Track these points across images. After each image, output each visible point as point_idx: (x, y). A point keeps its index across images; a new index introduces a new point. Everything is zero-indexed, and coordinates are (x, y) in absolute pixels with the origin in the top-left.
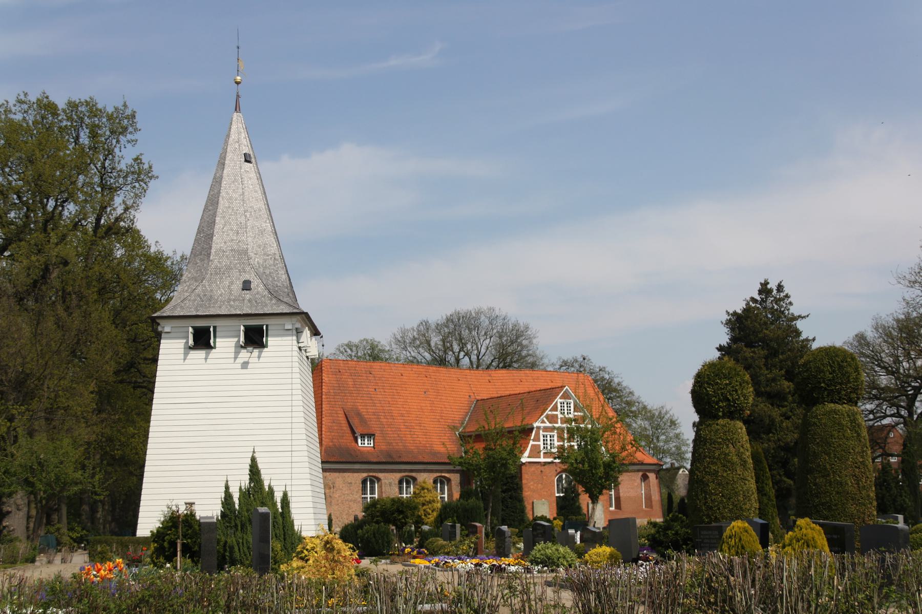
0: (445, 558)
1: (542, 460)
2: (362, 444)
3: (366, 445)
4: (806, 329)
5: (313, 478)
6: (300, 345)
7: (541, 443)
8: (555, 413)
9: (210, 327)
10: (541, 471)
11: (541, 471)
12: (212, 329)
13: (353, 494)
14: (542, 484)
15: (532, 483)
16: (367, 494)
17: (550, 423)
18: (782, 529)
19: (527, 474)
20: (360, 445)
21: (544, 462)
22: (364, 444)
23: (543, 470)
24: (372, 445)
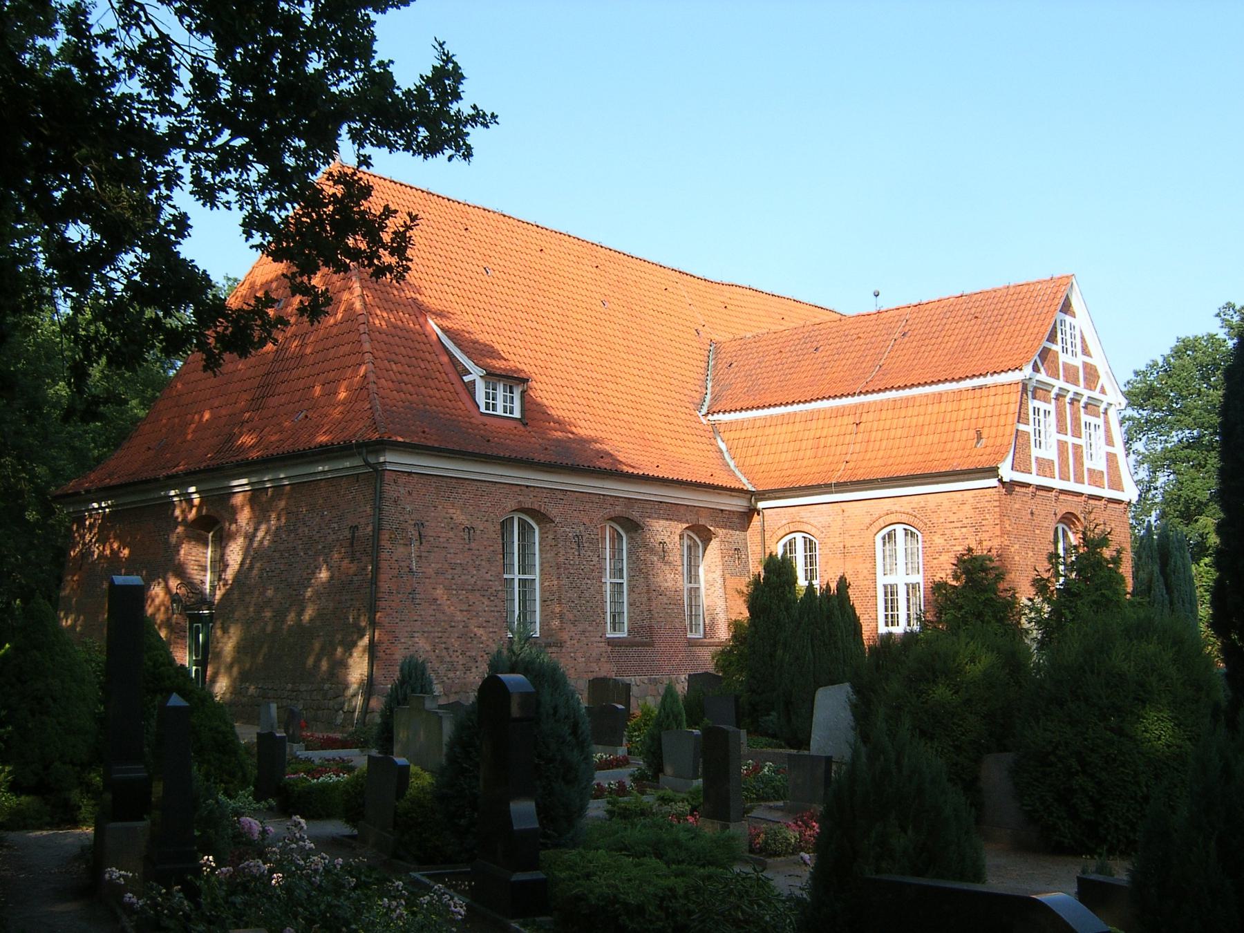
3: (500, 412)
13: (478, 568)
24: (517, 414)
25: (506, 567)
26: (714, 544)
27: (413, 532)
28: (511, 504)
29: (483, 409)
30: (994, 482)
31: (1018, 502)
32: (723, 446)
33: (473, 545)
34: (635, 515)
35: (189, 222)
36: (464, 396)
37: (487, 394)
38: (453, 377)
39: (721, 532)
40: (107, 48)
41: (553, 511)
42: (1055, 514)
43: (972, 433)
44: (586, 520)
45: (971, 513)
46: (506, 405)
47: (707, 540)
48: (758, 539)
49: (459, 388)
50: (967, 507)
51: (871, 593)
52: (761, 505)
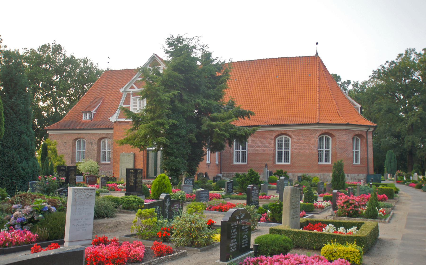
17: (138, 88)
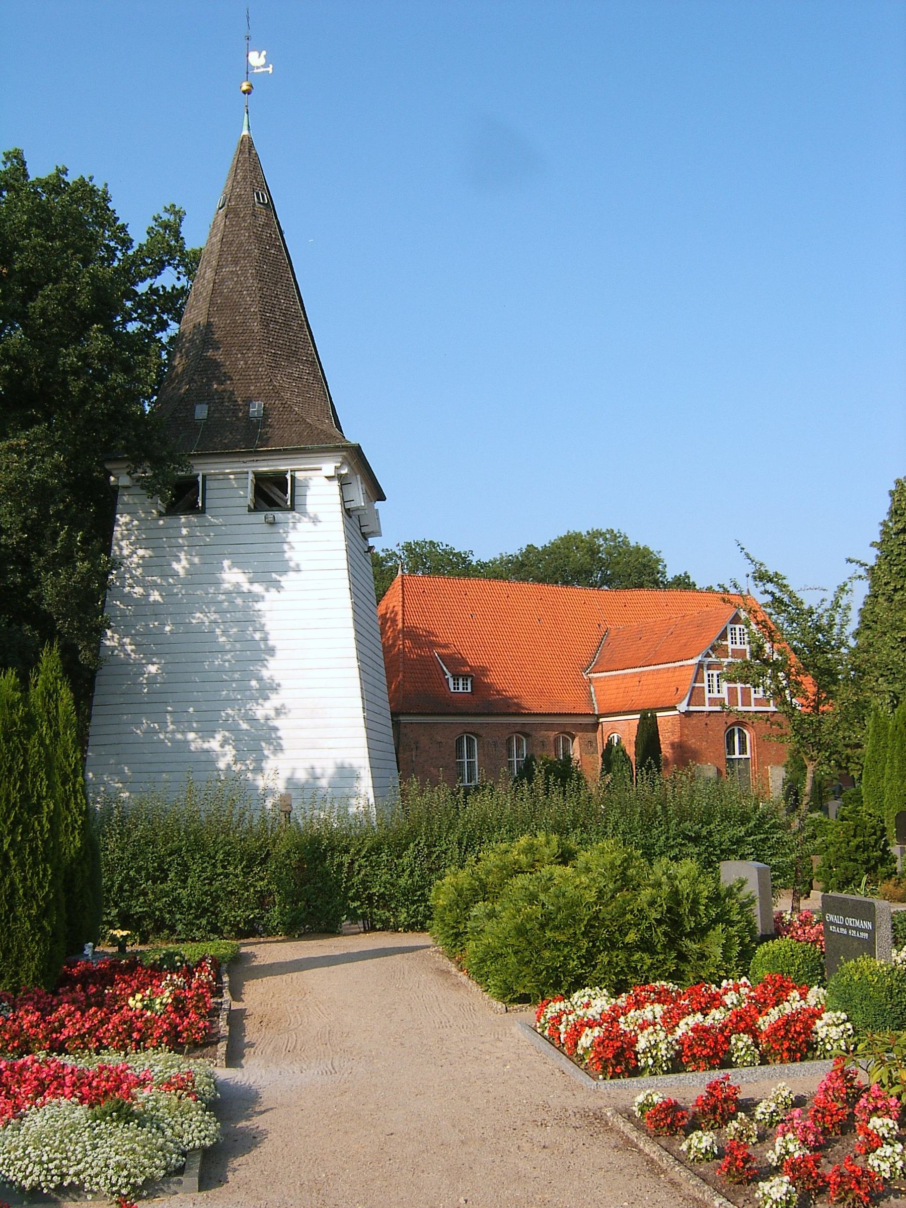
0: (338, 894)
1: (707, 708)
2: (455, 689)
3: (461, 690)
4: (251, 982)
5: (376, 709)
6: (348, 506)
7: (706, 685)
8: (724, 643)
9: (198, 475)
10: (706, 724)
11: (706, 724)
12: (200, 479)
14: (707, 741)
15: (693, 741)
16: (462, 757)
18: (565, 857)
19: (687, 728)
20: (452, 690)
21: (710, 712)
22: (458, 689)
23: (708, 722)
24: (469, 690)
25: (462, 757)
26: (577, 739)
27: (414, 746)
28: (460, 731)
29: (452, 690)
30: (677, 712)
31: (694, 720)
32: (592, 689)
33: (442, 749)
34: (527, 730)
35: (242, 996)
36: (445, 685)
37: (454, 684)
38: (442, 676)
39: (579, 734)
40: (271, 651)
41: (481, 732)
42: (726, 723)
43: (674, 689)
44: (500, 735)
45: (671, 726)
46: (463, 688)
47: (573, 738)
48: (601, 736)
49: (444, 681)
50: (670, 723)
51: (760, 750)
52: (601, 720)
